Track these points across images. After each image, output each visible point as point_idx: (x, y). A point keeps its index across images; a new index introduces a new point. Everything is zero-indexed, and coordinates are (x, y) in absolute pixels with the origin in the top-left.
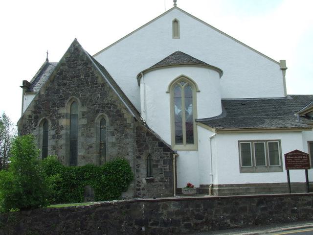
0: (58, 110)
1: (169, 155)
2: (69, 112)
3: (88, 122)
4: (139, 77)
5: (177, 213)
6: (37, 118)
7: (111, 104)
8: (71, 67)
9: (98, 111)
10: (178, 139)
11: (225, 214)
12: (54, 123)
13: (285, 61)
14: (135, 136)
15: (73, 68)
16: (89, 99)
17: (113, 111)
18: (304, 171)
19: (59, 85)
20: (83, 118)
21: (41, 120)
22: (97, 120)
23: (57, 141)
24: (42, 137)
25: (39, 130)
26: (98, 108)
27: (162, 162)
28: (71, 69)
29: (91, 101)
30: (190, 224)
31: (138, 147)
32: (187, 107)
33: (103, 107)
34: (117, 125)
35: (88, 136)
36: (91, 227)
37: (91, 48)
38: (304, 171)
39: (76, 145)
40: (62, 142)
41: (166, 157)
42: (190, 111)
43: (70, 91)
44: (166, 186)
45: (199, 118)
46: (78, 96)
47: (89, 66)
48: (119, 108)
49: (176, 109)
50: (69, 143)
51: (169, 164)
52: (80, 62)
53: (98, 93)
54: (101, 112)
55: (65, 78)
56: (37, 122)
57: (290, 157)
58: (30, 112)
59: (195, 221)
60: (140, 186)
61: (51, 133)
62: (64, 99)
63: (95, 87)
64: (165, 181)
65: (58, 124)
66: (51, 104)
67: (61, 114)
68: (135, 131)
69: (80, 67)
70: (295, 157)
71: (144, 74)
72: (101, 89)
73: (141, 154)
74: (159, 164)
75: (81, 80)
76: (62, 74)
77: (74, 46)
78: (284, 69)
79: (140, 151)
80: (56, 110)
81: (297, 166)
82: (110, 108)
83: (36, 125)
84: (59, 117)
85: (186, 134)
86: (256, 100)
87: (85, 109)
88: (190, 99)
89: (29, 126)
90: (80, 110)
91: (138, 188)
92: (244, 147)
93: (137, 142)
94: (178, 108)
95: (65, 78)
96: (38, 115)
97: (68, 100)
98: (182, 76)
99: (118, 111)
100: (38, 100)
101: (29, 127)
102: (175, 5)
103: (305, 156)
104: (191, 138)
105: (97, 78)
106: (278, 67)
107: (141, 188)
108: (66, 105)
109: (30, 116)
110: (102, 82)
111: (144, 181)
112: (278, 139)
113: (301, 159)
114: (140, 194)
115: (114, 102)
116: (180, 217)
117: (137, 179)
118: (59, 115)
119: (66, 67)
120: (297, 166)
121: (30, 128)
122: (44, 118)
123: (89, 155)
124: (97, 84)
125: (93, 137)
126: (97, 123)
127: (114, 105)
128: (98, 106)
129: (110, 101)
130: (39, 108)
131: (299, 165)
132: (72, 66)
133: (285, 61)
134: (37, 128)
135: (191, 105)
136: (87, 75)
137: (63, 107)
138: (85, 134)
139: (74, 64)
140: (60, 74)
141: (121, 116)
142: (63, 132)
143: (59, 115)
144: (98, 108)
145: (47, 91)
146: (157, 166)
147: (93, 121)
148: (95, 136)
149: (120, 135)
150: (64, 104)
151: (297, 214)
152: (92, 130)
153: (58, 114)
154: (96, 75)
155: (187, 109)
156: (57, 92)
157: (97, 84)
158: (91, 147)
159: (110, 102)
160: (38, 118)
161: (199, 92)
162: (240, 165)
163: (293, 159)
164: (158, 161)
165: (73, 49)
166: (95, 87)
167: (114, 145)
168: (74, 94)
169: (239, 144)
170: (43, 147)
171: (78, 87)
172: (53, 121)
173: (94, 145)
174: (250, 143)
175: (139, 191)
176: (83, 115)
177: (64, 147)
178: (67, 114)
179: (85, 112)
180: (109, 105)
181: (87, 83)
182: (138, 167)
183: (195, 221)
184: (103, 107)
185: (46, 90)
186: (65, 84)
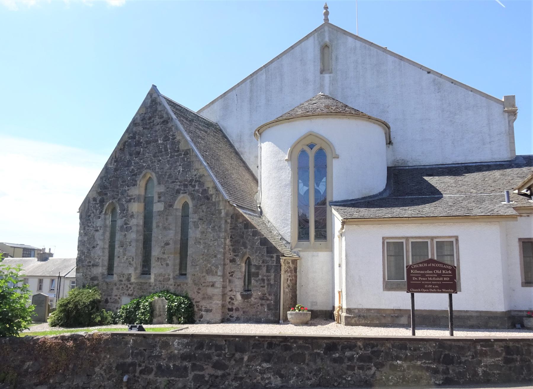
0: (128, 190)
1: (275, 259)
2: (143, 193)
3: (165, 208)
4: (386, 126)
5: (184, 357)
6: (102, 202)
7: (196, 181)
8: (146, 128)
9: (178, 192)
10: (303, 232)
11: (265, 365)
12: (123, 210)
13: (514, 97)
14: (229, 228)
15: (148, 129)
16: (168, 174)
17: (198, 191)
18: (447, 295)
19: (131, 155)
20: (159, 202)
21: (108, 204)
22: (178, 205)
23: (125, 235)
24: (108, 229)
25: (105, 219)
26: (178, 187)
27: (264, 269)
28: (146, 131)
29: (170, 176)
30: (203, 376)
31: (232, 246)
32: (318, 181)
33: (186, 186)
34: (203, 211)
35: (165, 228)
36: (101, 368)
37: (193, 95)
38: (447, 295)
39: (151, 241)
40: (132, 236)
41: (270, 262)
42: (322, 188)
43: (143, 162)
44: (269, 306)
45: (335, 199)
46: (154, 170)
47: (170, 125)
48: (205, 187)
49: (301, 185)
50: (141, 237)
51: (274, 272)
52: (157, 120)
53: (180, 165)
54: (183, 193)
55: (138, 144)
56: (102, 206)
57: (416, 272)
58: (95, 192)
59: (212, 371)
60: (233, 304)
61: (120, 222)
62: (135, 175)
63: (176, 156)
64: (268, 299)
65: (127, 210)
66: (120, 182)
67: (132, 195)
68: (229, 221)
69: (158, 127)
70: (428, 272)
71: (260, 134)
72: (183, 159)
73: (235, 256)
74: (260, 272)
75: (158, 146)
76: (135, 138)
77: (151, 96)
78: (513, 114)
79: (234, 251)
80: (125, 191)
81: (430, 286)
82: (194, 186)
83: (102, 212)
84: (130, 201)
85: (313, 227)
86: (441, 168)
87: (162, 189)
88: (322, 168)
89: (93, 212)
90: (157, 189)
91: (230, 307)
92: (393, 249)
93: (231, 237)
94: (304, 185)
95: (138, 144)
96: (105, 197)
97: (141, 176)
98: (310, 134)
99: (205, 191)
100: (105, 176)
101: (92, 215)
102: (326, 20)
103: (448, 270)
104: (323, 232)
105: (179, 142)
106: (497, 110)
107: (234, 308)
108: (138, 182)
109: (95, 199)
110: (186, 148)
111: (239, 297)
112: (455, 234)
113: (439, 276)
114: (233, 317)
115: (200, 177)
116: (188, 364)
117: (229, 293)
118: (129, 198)
119: (141, 128)
120: (430, 286)
121: (94, 216)
122: (111, 201)
123: (165, 256)
124: (178, 151)
125: (170, 229)
126: (176, 209)
127: (200, 181)
128: (179, 183)
129: (195, 175)
130: (105, 187)
131: (433, 285)
132: (148, 127)
133: (514, 97)
134: (102, 216)
135: (324, 180)
136: (166, 139)
137: (134, 185)
138: (161, 225)
139: (151, 122)
140: (133, 138)
141: (208, 199)
142: (133, 222)
143: (129, 198)
144: (178, 187)
145: (115, 164)
146: (257, 275)
147: (171, 206)
148: (174, 229)
149: (206, 227)
150: (136, 181)
151: (400, 373)
152: (170, 218)
153: (128, 196)
154: (178, 138)
155: (318, 186)
156: (129, 164)
157: (178, 151)
158: (167, 244)
159: (194, 179)
160: (104, 202)
161: (338, 157)
162: (384, 279)
163: (423, 276)
164: (258, 267)
165: (149, 101)
166: (176, 156)
167: (197, 242)
168: (149, 167)
169: (383, 243)
170: (110, 242)
171: (154, 156)
172: (122, 206)
173: (171, 242)
174: (429, 241)
175: (231, 313)
176: (159, 197)
177: (134, 244)
178: (139, 196)
179: (161, 193)
180: (193, 183)
181: (166, 150)
182: (232, 276)
183: (212, 371)
184: (186, 186)
185: (115, 162)
186: (138, 153)
